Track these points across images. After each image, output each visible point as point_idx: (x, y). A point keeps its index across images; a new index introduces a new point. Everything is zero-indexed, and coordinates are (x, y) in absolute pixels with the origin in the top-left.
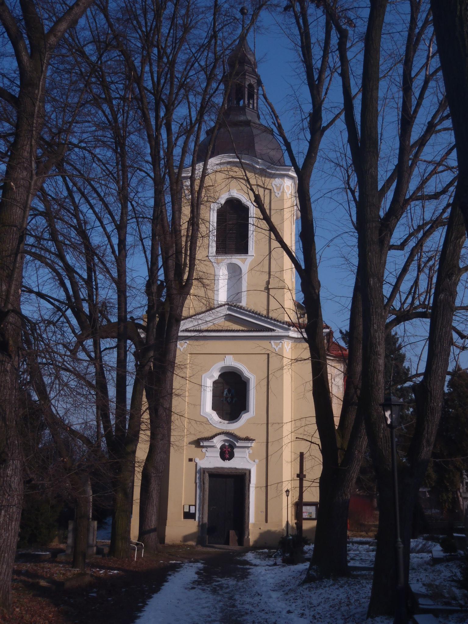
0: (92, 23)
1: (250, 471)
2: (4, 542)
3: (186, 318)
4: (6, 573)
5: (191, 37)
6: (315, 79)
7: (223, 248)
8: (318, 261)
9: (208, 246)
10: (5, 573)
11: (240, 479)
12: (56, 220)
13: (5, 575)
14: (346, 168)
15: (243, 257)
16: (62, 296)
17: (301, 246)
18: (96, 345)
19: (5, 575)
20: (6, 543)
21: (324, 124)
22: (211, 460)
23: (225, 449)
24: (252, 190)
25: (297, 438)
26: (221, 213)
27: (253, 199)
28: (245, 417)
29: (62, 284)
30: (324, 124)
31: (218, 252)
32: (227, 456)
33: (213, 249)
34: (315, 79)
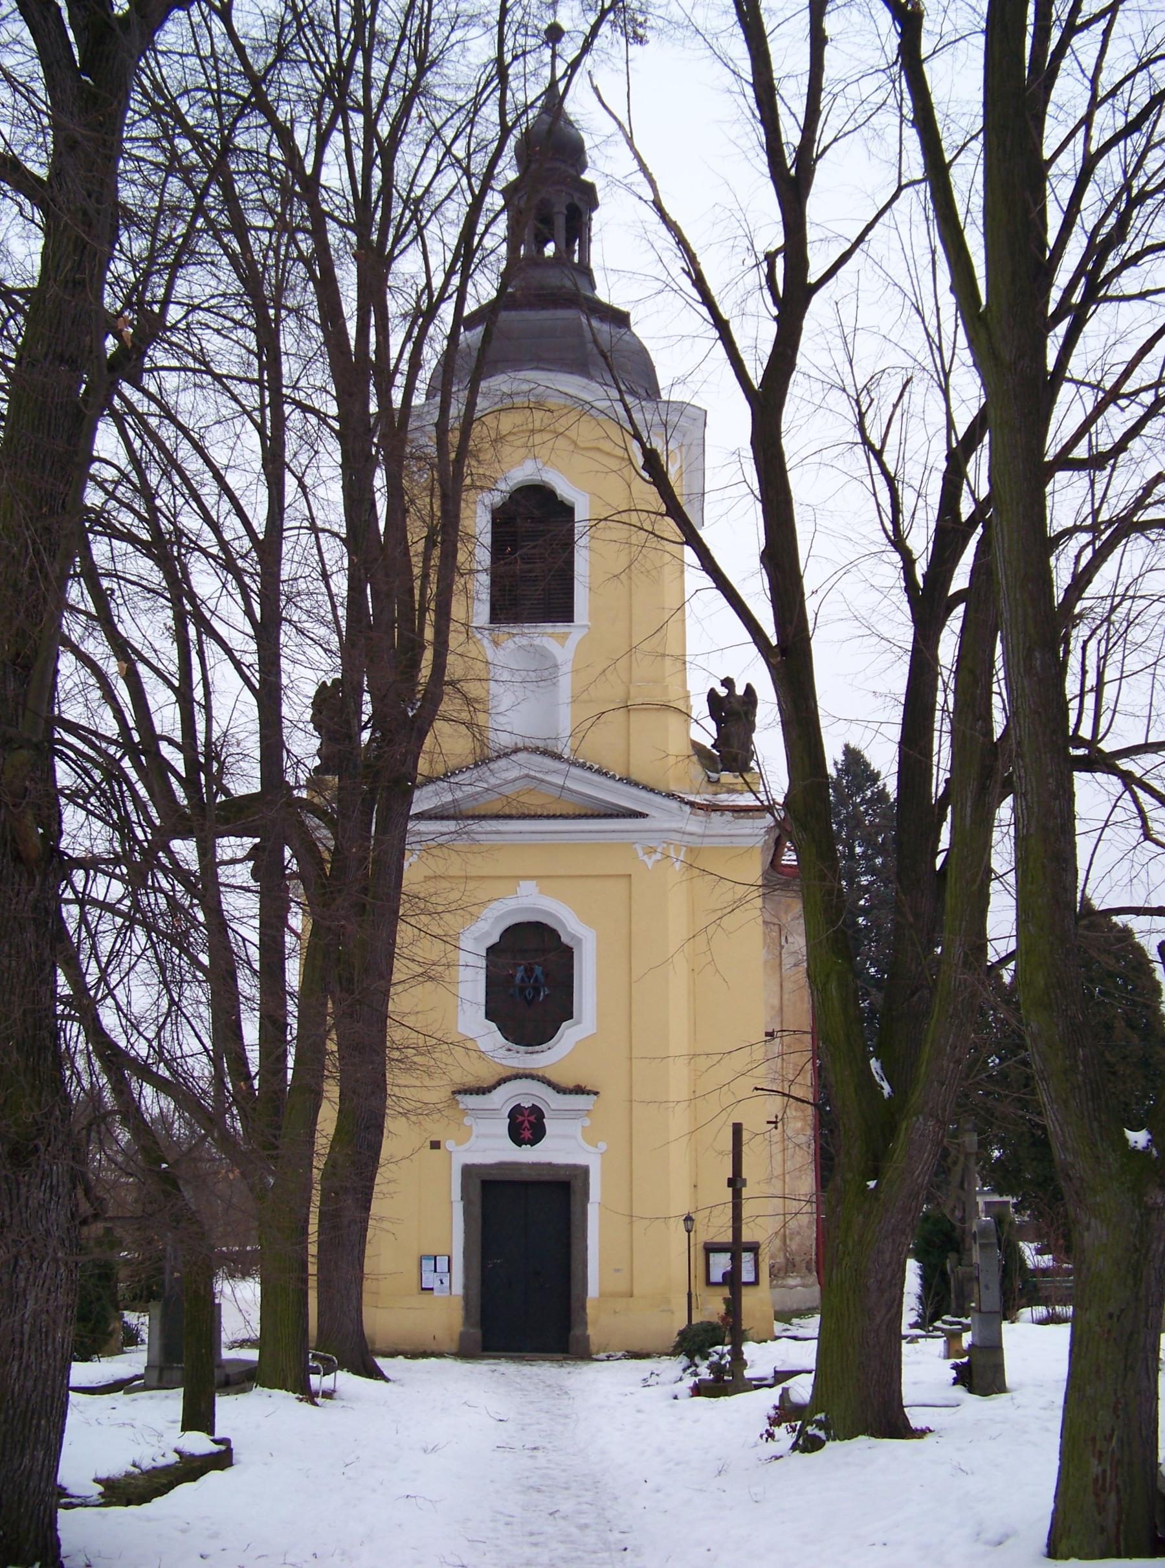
0: (202, 36)
1: (584, 1171)
2: (35, 1386)
3: (430, 780)
4: (45, 1472)
5: (437, 80)
6: (789, 165)
7: (510, 607)
8: (811, 626)
9: (474, 601)
10: (41, 1473)
11: (562, 1191)
12: (91, 536)
13: (40, 1480)
14: (853, 393)
15: (561, 628)
16: (109, 726)
17: (767, 586)
18: (206, 852)
19: (40, 1480)
20: (40, 1387)
21: (812, 278)
22: (492, 1146)
23: (521, 1118)
24: (637, 436)
25: (757, 1089)
26: (502, 519)
27: (639, 461)
28: (569, 1036)
29: (109, 696)
30: (812, 278)
31: (494, 618)
32: (527, 1134)
33: (482, 612)
34: (789, 165)
